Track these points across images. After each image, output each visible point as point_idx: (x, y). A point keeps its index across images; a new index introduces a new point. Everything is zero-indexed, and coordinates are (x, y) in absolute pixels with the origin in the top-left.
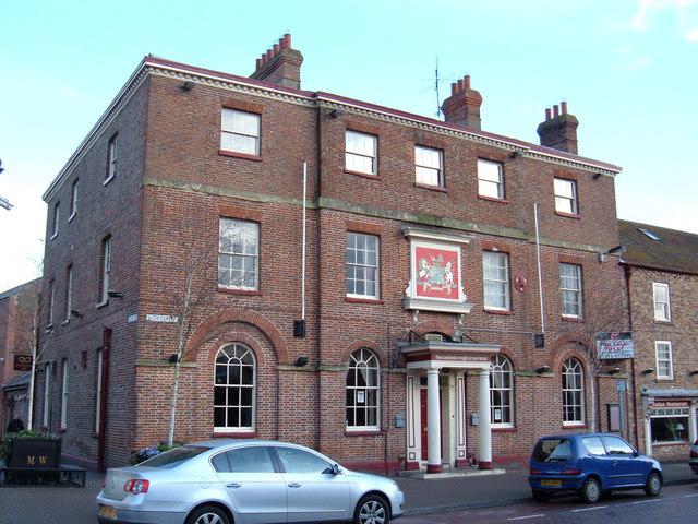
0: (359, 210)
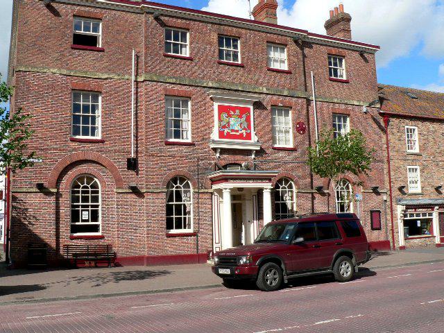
0: (174, 81)
